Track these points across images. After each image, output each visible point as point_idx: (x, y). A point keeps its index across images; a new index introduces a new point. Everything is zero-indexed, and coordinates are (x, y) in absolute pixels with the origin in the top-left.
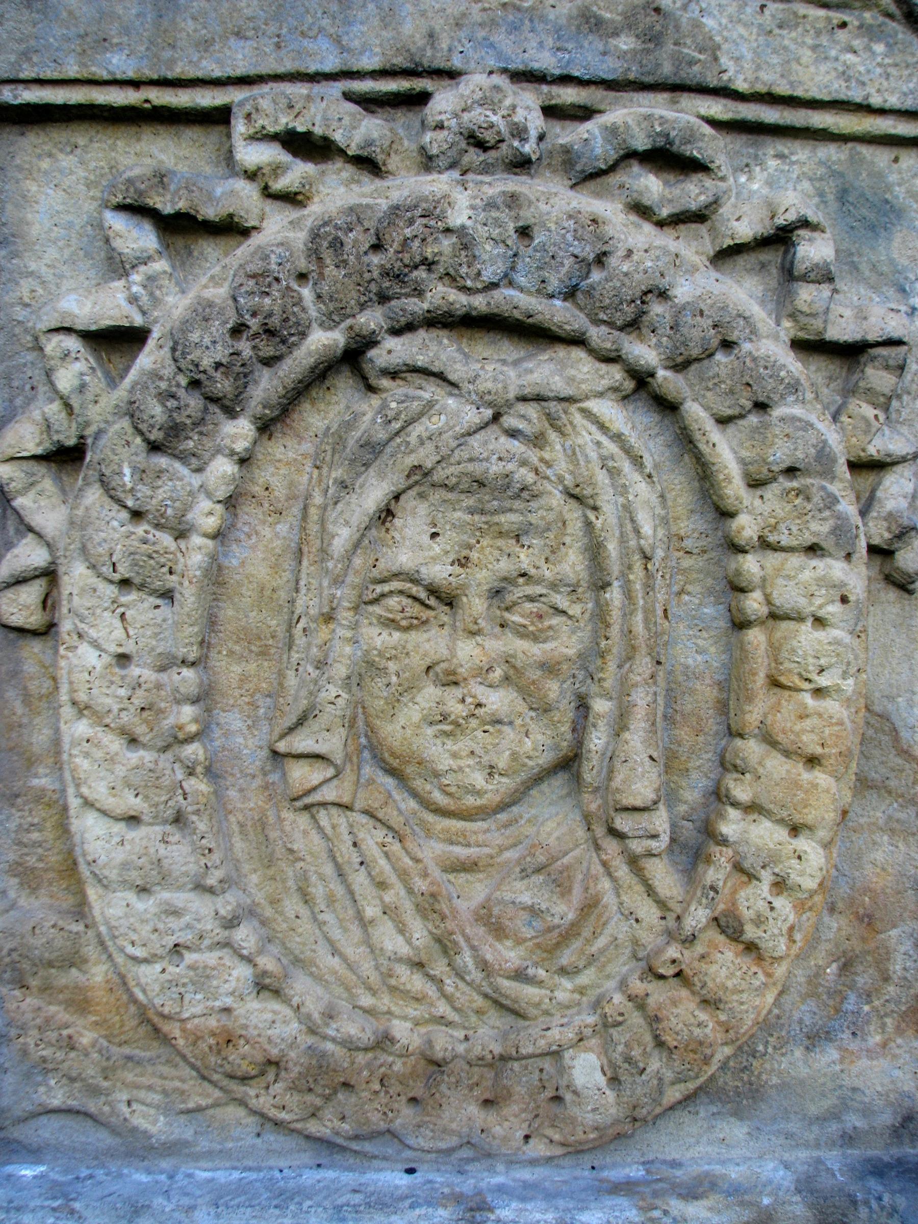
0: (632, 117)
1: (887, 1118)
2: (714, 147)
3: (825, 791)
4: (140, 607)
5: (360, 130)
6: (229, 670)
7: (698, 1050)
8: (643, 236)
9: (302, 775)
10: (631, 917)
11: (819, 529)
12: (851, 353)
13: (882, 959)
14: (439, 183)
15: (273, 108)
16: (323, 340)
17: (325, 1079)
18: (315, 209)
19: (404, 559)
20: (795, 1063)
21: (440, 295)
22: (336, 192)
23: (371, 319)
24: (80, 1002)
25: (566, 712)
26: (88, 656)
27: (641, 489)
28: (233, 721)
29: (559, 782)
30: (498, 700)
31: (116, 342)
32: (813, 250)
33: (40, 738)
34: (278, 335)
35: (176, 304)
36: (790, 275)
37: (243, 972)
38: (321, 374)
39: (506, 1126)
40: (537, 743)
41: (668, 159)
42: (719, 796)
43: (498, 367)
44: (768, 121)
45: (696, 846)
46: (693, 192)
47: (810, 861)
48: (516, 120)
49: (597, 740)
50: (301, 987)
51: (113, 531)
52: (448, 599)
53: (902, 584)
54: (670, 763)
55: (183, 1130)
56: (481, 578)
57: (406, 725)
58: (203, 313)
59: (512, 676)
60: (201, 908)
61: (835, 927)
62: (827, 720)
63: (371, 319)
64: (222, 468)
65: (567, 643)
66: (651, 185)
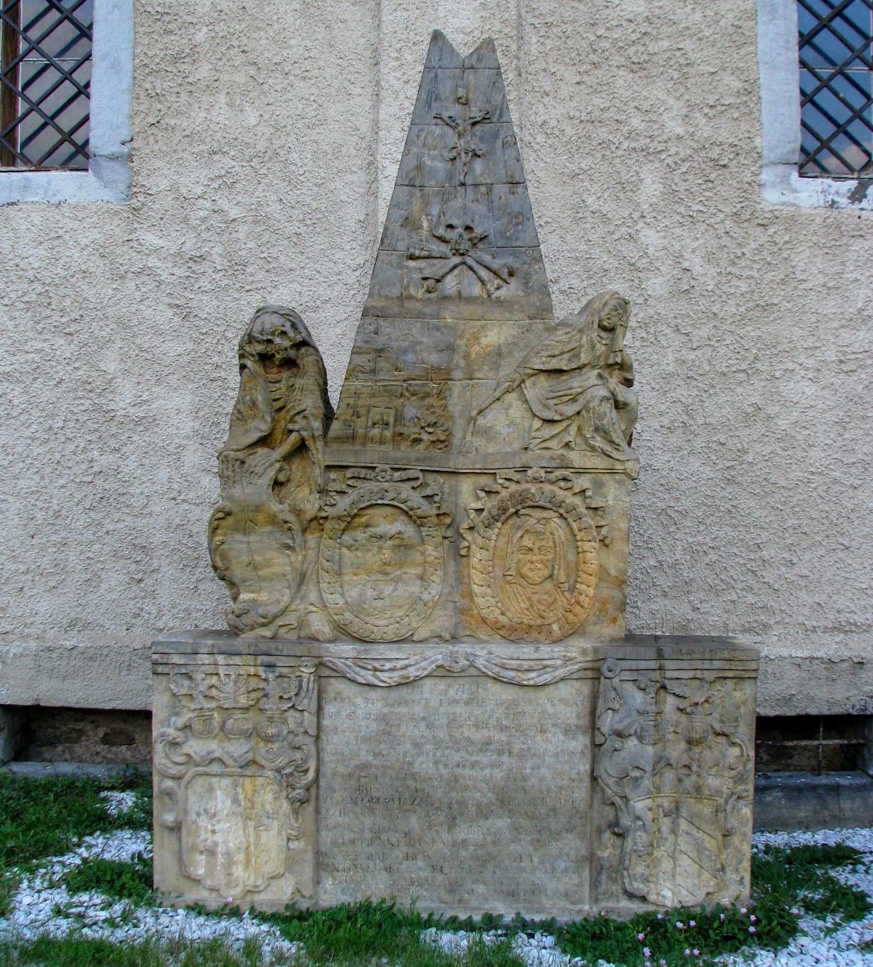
0: (559, 473)
1: (608, 639)
2: (572, 476)
3: (593, 580)
4: (483, 552)
5: (517, 477)
6: (497, 562)
7: (574, 624)
8: (561, 492)
9: (509, 578)
10: (562, 602)
11: (590, 538)
12: (596, 509)
13: (606, 610)
14: (529, 485)
15: (504, 473)
16: (512, 510)
17: (513, 629)
18: (510, 490)
19: (525, 544)
20: (591, 628)
21: (530, 503)
22: (513, 487)
23: (519, 507)
24: (472, 616)
25: (550, 567)
26: (475, 560)
27: (562, 532)
28: (497, 570)
29: (549, 580)
30: (539, 566)
31: (480, 511)
32: (588, 493)
33: (465, 573)
34: (505, 510)
35: (489, 505)
36: (585, 498)
37: (498, 611)
38: (511, 516)
39: (542, 637)
40: (546, 573)
41: (565, 479)
42: (576, 581)
43: (539, 514)
44: (580, 472)
45: (572, 589)
46: (569, 485)
47: (591, 591)
48: (520, 293)
49: (556, 572)
50: (508, 614)
51: (480, 540)
52: (531, 550)
53: (607, 546)
54: (568, 576)
55: (489, 638)
56: (537, 546)
57: (525, 570)
58: (493, 507)
59: (542, 562)
60: (492, 600)
61: (597, 604)
62: (593, 567)
63: (519, 507)
64: (497, 530)
65: (550, 557)
66: (562, 484)
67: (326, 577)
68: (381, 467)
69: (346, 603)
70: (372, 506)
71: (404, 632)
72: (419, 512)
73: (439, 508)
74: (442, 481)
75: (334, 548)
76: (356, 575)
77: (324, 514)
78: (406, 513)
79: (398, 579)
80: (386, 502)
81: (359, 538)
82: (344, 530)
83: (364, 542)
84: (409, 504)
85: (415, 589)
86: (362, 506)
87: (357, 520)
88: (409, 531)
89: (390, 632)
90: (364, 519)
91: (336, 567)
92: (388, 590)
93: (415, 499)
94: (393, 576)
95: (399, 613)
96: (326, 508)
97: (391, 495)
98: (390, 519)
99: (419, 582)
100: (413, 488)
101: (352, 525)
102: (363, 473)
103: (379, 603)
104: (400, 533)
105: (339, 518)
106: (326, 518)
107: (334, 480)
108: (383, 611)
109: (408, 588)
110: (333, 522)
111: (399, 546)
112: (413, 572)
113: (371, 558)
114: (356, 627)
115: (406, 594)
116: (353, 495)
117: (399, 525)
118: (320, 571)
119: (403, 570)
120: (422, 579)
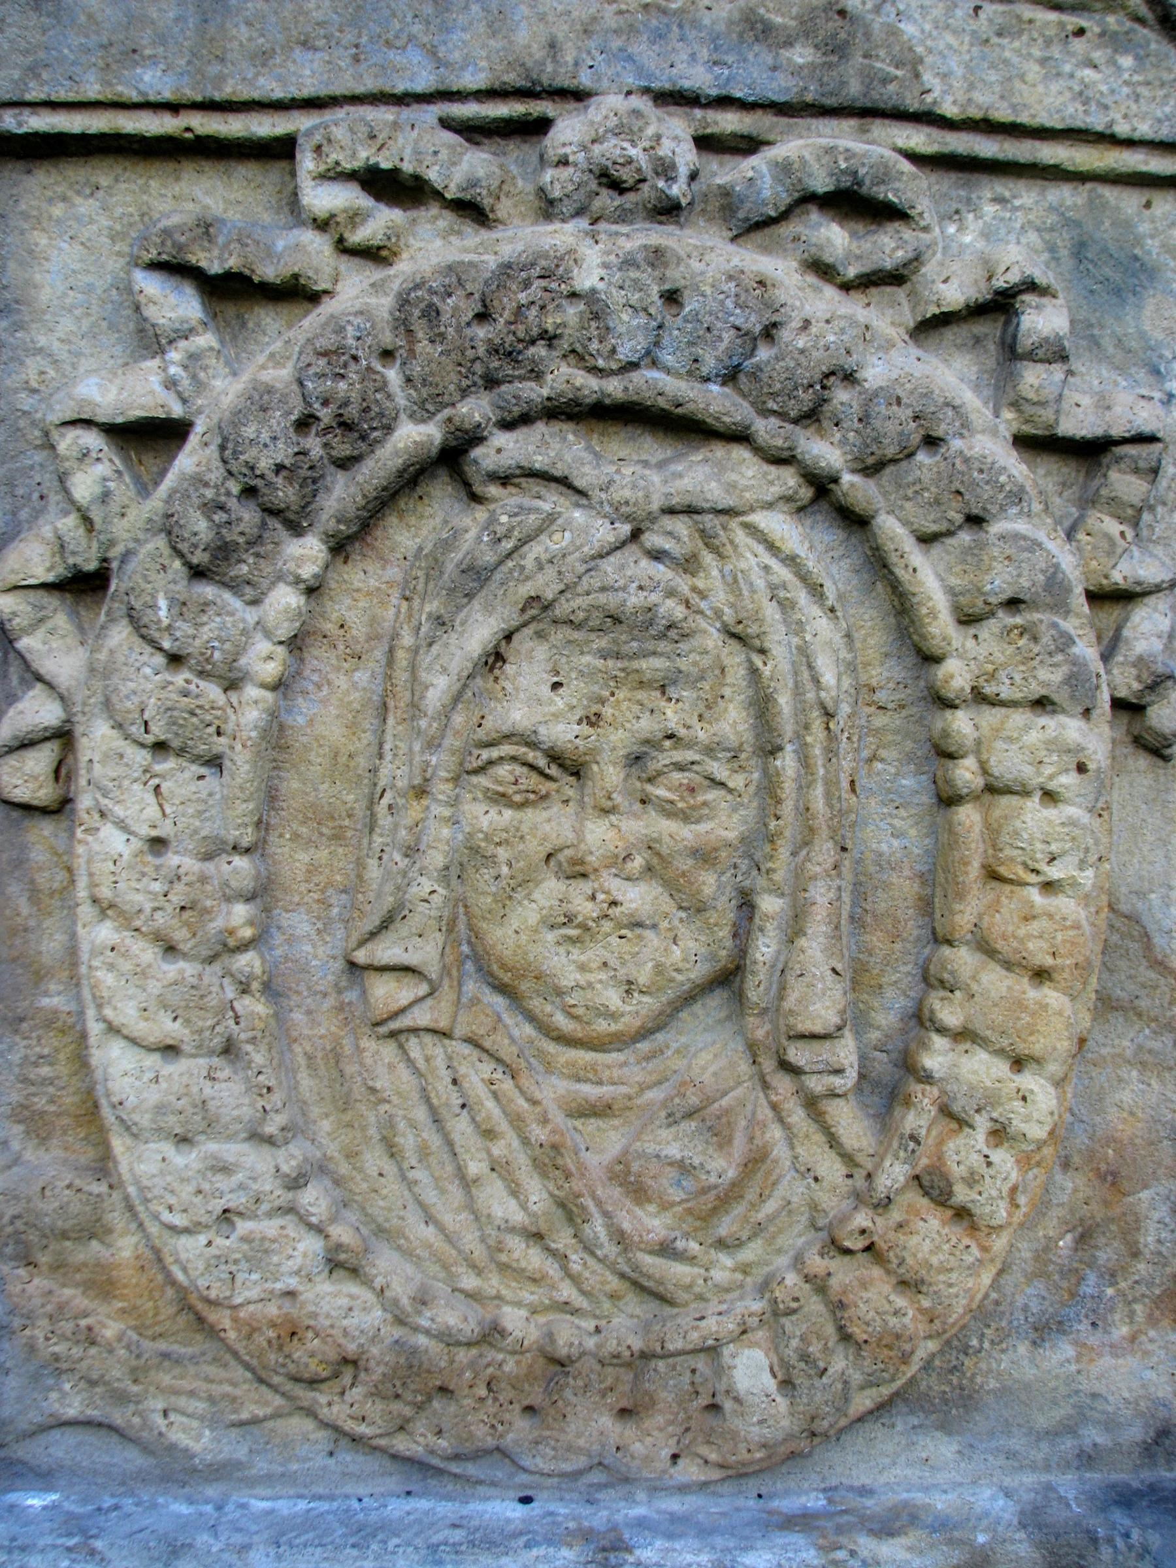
0: (810, 150)
1: (1136, 1433)
2: (914, 189)
3: (1057, 1013)
4: (180, 777)
5: (461, 166)
7: (895, 1345)
8: (823, 302)
9: (387, 993)
10: (808, 1174)
11: (1049, 678)
12: (1090, 452)
13: (1130, 1228)
14: (562, 235)
15: (350, 138)
16: (414, 435)
17: (417, 1383)
18: (403, 268)
19: (518, 716)
20: (1018, 1362)
21: (564, 378)
22: (431, 245)
23: (476, 409)
24: (103, 1284)
25: (725, 912)
26: (113, 840)
27: (821, 626)
29: (716, 1002)
30: (638, 897)
31: (148, 438)
32: (1042, 320)
33: (51, 946)
34: (357, 429)
35: (226, 390)
36: (1012, 352)
38: (411, 479)
40: (688, 952)
41: (855, 203)
43: (638, 471)
44: (984, 154)
45: (892, 1083)
46: (888, 246)
47: (1038, 1103)
49: (765, 948)
50: (386, 1264)
51: (145, 681)
52: (574, 767)
53: (1155, 748)
54: (859, 977)
55: (234, 1448)
56: (616, 740)
57: (520, 929)
58: (260, 401)
59: (656, 865)
60: (258, 1163)
62: (1059, 922)
63: (476, 409)
65: (726, 824)
66: (834, 237)
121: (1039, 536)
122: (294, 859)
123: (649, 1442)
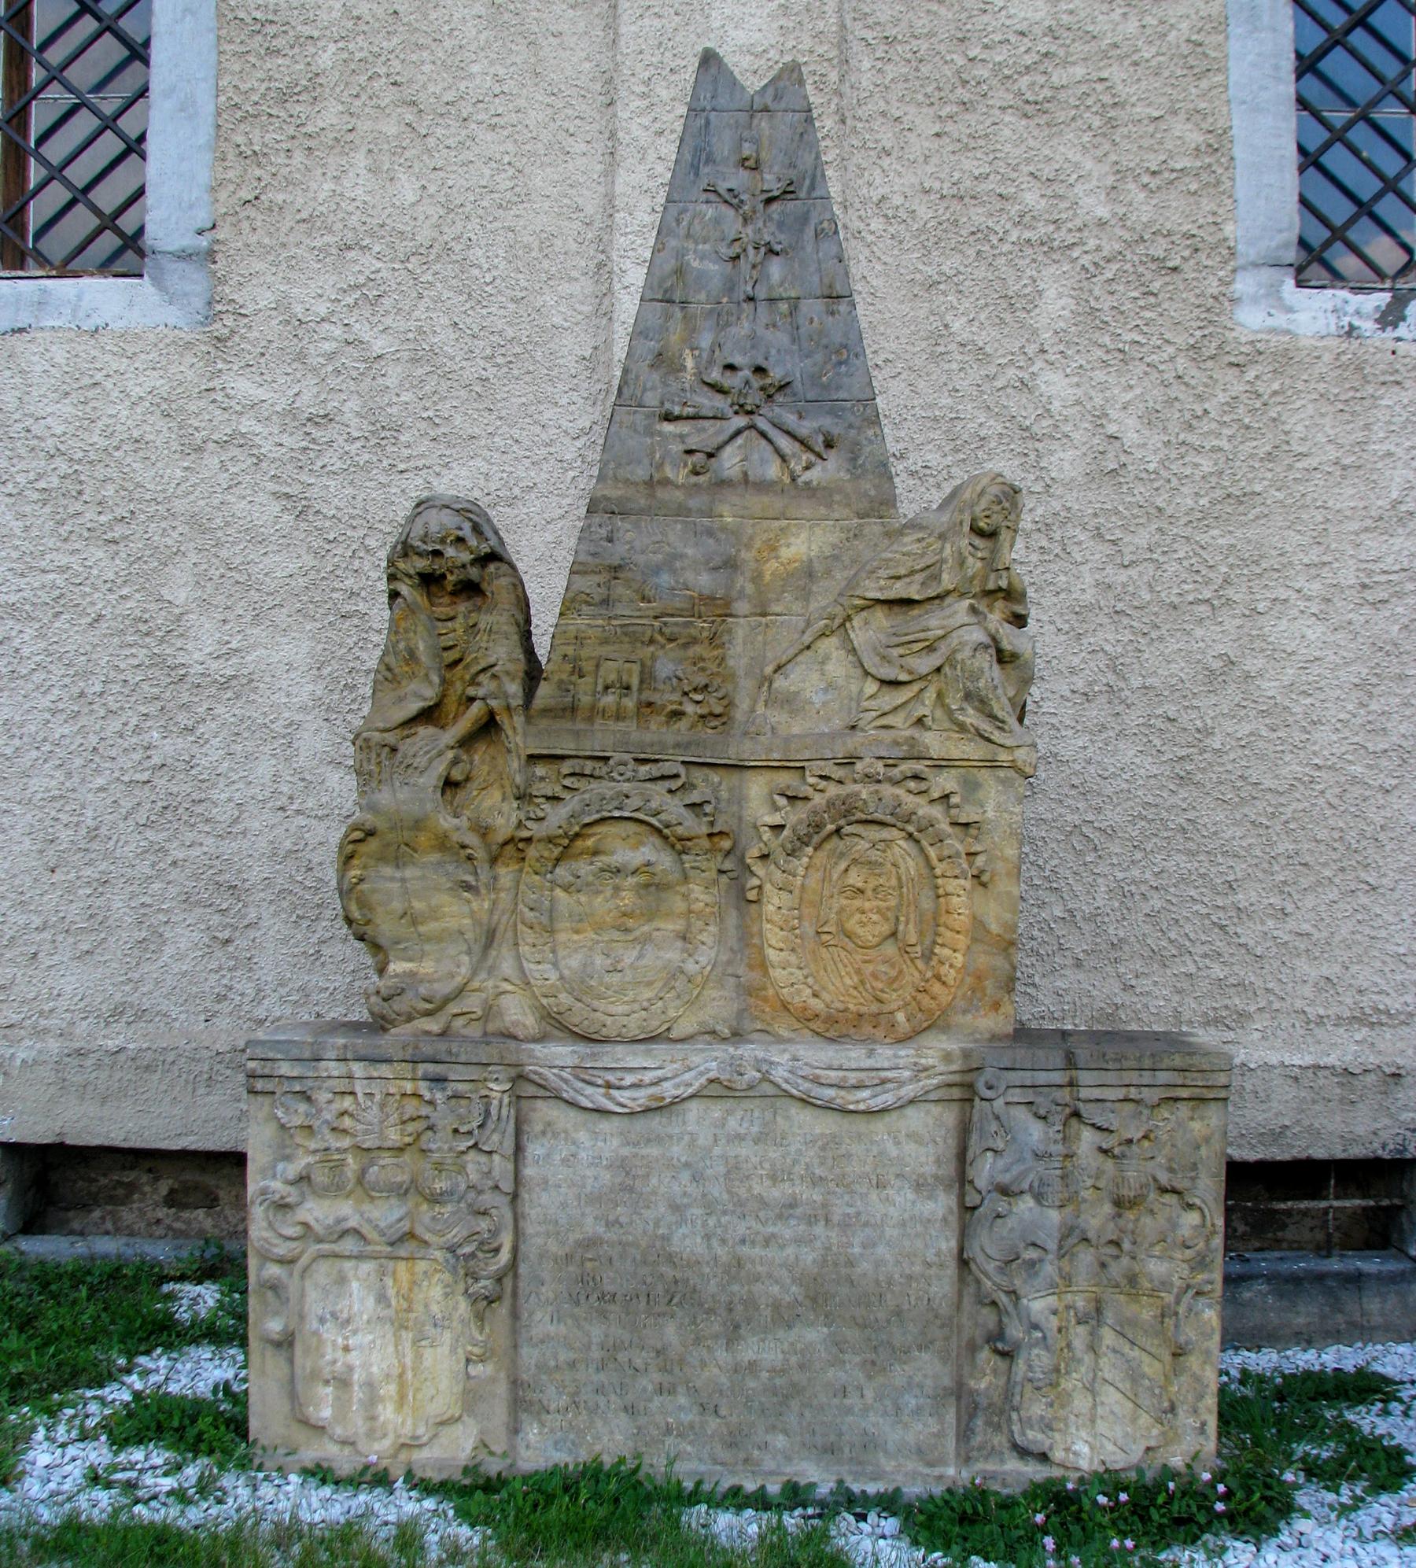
0: (907, 767)
1: (987, 1036)
2: (927, 772)
3: (962, 941)
4: (784, 895)
5: (838, 773)
7: (930, 1011)
8: (910, 798)
9: (825, 937)
10: (912, 976)
11: (957, 872)
12: (967, 825)
13: (983, 989)
14: (857, 787)
15: (818, 767)
16: (831, 827)
17: (831, 1020)
18: (827, 795)
19: (851, 881)
20: (959, 1019)
21: (860, 816)
22: (833, 790)
23: (842, 822)
24: (765, 999)
25: (893, 920)
26: (771, 908)
27: (911, 863)
28: (806, 924)
29: (891, 941)
30: (875, 917)
31: (778, 828)
32: (954, 800)
33: (755, 929)
34: (819, 827)
35: (793, 819)
36: (949, 807)
38: (829, 836)
40: (886, 929)
41: (916, 777)
42: (935, 943)
43: (874, 833)
44: (941, 765)
45: (928, 956)
46: (923, 786)
47: (959, 959)
49: (901, 928)
50: (824, 995)
51: (778, 876)
52: (861, 891)
53: (984, 885)
54: (921, 933)
55: (792, 1035)
56: (871, 886)
57: (851, 924)
58: (800, 821)
59: (879, 911)
60: (799, 973)
61: (969, 980)
62: (961, 920)
63: (842, 822)
64: (805, 860)
65: (893, 903)
66: (912, 784)
67: (529, 936)
68: (617, 757)
69: (562, 978)
70: (603, 820)
71: (655, 1025)
72: (680, 830)
73: (712, 823)
74: (716, 779)
75: (542, 888)
76: (577, 932)
77: (525, 834)
78: (659, 831)
79: (646, 939)
80: (626, 814)
81: (582, 873)
82: (558, 860)
83: (591, 878)
84: (663, 816)
85: (673, 954)
86: (587, 820)
87: (579, 844)
88: (664, 860)
89: (632, 1025)
90: (590, 842)
91: (545, 920)
92: (629, 956)
93: (674, 809)
94: (637, 933)
95: (648, 994)
96: (529, 824)
97: (635, 802)
98: (632, 841)
99: (679, 944)
100: (670, 791)
101: (572, 851)
102: (589, 767)
103: (615, 978)
104: (648, 864)
105: (550, 840)
106: (529, 840)
107: (542, 779)
108: (622, 990)
109: (661, 954)
110: (541, 846)
111: (647, 886)
112: (671, 927)
113: (602, 904)
114: (577, 1017)
115: (659, 963)
116: (572, 803)
117: (648, 852)
118: (520, 926)
119: (654, 924)
120: (684, 938)
121: (955, 844)
122: (806, 911)
123: (879, 1033)
